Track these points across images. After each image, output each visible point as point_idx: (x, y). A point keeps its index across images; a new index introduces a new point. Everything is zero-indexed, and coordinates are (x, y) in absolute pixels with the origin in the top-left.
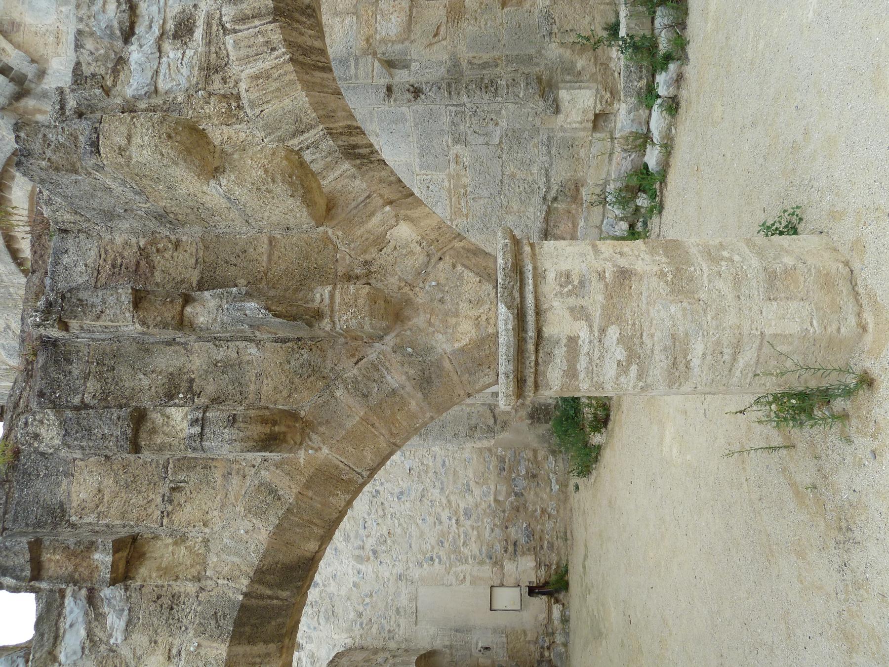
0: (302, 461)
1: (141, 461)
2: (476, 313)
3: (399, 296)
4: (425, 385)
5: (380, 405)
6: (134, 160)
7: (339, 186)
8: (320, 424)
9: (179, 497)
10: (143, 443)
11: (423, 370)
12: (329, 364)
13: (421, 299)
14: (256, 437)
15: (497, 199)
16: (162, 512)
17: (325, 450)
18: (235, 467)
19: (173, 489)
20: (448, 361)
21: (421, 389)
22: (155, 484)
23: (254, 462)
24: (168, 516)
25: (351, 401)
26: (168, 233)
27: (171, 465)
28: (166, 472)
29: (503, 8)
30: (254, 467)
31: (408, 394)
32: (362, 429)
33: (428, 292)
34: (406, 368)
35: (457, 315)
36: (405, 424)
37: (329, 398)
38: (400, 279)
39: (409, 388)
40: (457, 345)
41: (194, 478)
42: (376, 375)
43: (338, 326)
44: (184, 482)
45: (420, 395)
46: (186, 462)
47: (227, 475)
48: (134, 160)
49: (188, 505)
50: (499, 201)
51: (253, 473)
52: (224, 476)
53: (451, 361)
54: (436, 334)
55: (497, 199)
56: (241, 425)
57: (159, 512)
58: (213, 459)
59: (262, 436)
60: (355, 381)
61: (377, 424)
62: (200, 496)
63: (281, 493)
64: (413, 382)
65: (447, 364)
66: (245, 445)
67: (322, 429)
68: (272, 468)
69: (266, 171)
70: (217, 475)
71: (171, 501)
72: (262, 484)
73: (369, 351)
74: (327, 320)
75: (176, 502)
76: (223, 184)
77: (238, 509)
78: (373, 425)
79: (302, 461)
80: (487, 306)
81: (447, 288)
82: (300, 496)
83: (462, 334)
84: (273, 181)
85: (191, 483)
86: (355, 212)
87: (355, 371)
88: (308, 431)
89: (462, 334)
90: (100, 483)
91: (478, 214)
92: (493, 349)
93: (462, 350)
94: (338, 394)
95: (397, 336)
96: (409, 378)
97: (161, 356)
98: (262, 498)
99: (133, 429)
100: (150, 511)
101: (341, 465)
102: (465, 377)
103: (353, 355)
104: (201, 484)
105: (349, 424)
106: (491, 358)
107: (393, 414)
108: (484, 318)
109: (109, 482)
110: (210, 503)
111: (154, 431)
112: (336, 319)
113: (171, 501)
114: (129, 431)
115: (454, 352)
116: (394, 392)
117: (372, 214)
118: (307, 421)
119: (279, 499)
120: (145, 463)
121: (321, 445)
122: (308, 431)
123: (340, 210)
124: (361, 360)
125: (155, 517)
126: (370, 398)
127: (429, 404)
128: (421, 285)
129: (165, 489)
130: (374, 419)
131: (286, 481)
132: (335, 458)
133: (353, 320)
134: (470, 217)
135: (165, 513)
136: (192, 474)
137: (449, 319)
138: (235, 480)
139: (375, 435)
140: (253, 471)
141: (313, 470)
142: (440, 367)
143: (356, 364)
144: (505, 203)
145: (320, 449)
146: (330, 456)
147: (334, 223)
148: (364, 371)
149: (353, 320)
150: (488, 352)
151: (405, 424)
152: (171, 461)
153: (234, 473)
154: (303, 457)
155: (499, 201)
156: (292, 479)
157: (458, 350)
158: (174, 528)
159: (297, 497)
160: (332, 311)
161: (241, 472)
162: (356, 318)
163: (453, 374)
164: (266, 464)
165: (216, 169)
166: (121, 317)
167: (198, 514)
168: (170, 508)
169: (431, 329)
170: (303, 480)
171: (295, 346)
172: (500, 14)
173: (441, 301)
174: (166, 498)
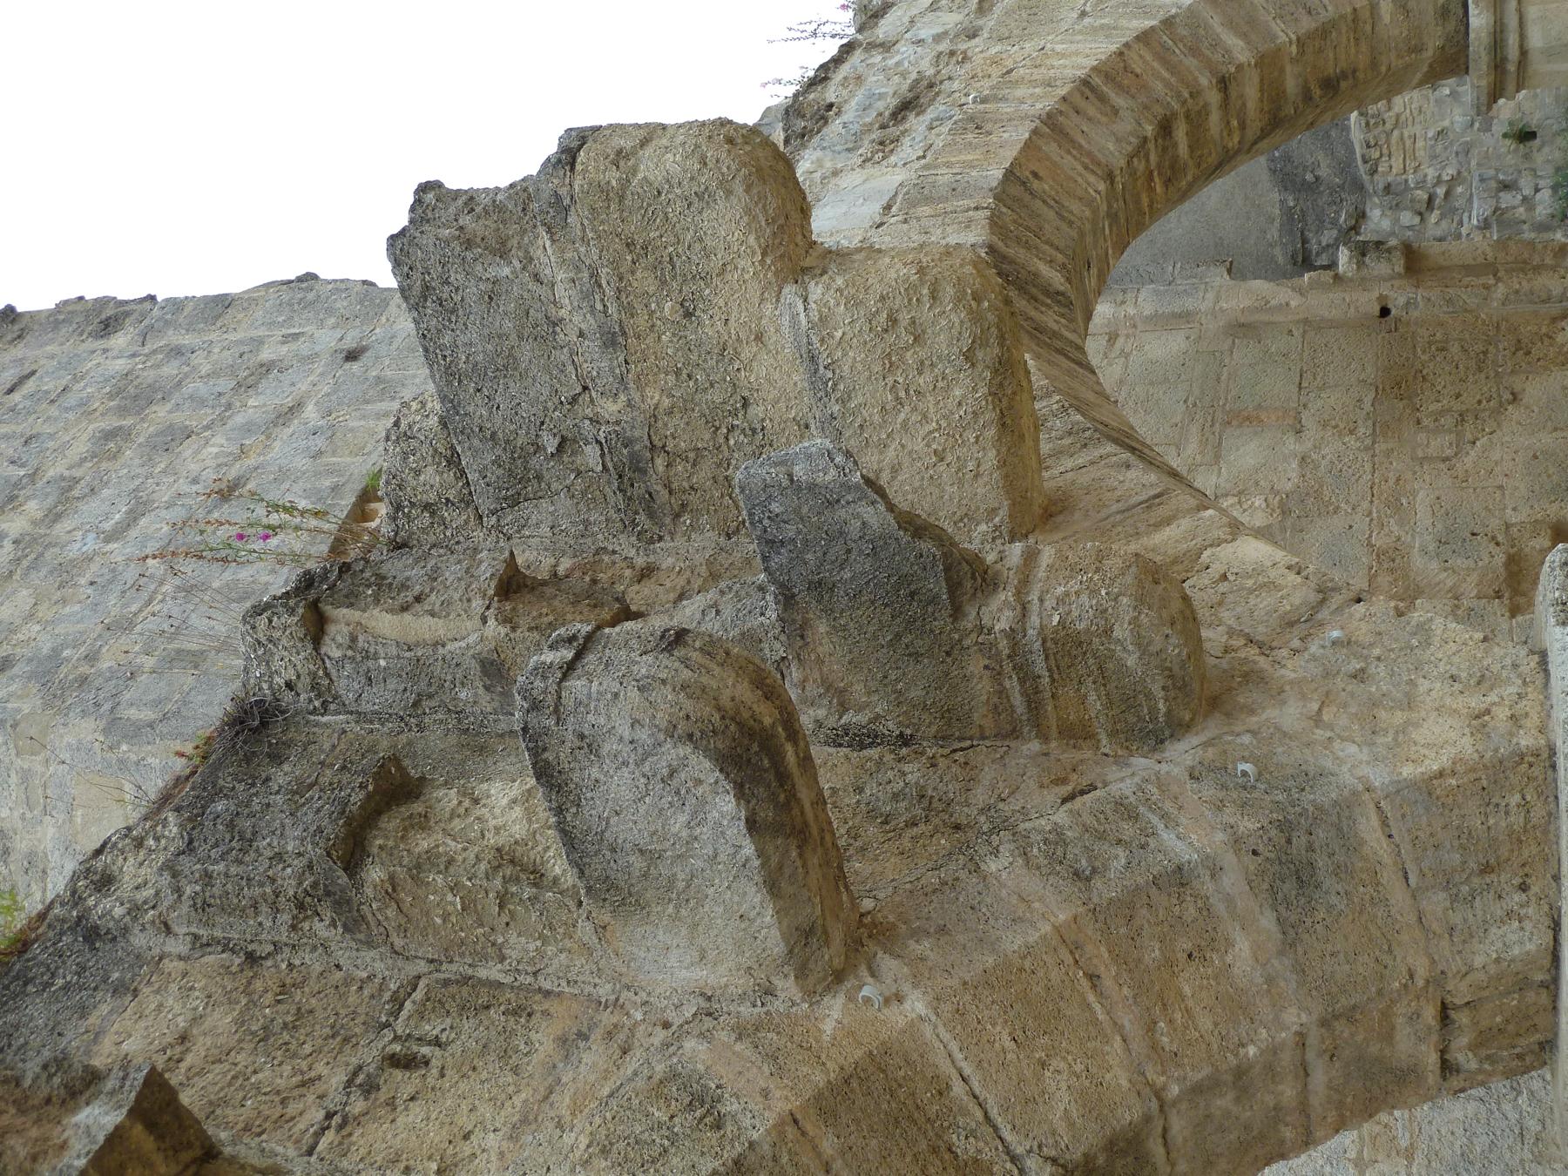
0: (828, 1027)
1: (339, 975)
2: (1476, 702)
3: (1224, 664)
4: (1289, 887)
5: (1126, 907)
6: (640, 176)
7: (1084, 478)
8: (917, 934)
9: (403, 1082)
10: (379, 842)
11: (1286, 827)
12: (980, 796)
13: (1292, 670)
14: (725, 700)
15: (1507, 1107)
16: (329, 1116)
17: (917, 1004)
18: (607, 1018)
19: (395, 1061)
20: (1375, 821)
21: (1275, 899)
22: (346, 1040)
23: (671, 1015)
24: (341, 1127)
25: (1032, 884)
26: (633, 553)
27: (418, 995)
28: (396, 1014)
29: (1513, 616)
30: (666, 1025)
31: (1229, 900)
32: (1055, 975)
33: (1314, 658)
34: (1230, 815)
35: (1410, 703)
36: (1205, 1023)
37: (962, 874)
38: (1231, 633)
39: (1233, 881)
40: (1407, 771)
41: (468, 1034)
42: (1128, 830)
43: (1034, 620)
44: (437, 1042)
45: (1268, 921)
46: (465, 990)
47: (570, 1043)
48: (640, 176)
49: (417, 1111)
50: (1513, 1116)
51: (657, 1041)
52: (563, 1041)
53: (1384, 823)
54: (1337, 745)
55: (1507, 1107)
56: (695, 655)
57: (321, 1114)
58: (547, 994)
59: (746, 715)
60: (1056, 838)
61: (1108, 982)
62: (463, 1086)
63: (730, 1106)
64: (1252, 863)
65: (1368, 826)
66: (688, 705)
67: (924, 947)
68: (723, 1036)
69: (921, 271)
70: (543, 1039)
71: (369, 1088)
72: (676, 1075)
73: (1113, 773)
74: (1005, 595)
75: (383, 1096)
76: (812, 298)
77: (569, 1139)
78: (1093, 978)
79: (828, 1027)
80: (1513, 690)
81: (1377, 652)
82: (791, 1132)
83: (1428, 746)
84: (934, 297)
85: (456, 1048)
86: (1118, 517)
87: (1062, 817)
88: (871, 947)
89: (1428, 746)
90: (196, 1020)
91: (1446, 1153)
92: (1538, 813)
93: (1427, 787)
94: (992, 866)
95: (1206, 745)
96: (1237, 841)
97: (513, 759)
98: (660, 1115)
99: (369, 796)
100: (292, 1109)
101: (958, 1088)
102: (1436, 902)
103: (1063, 781)
104: (482, 1055)
105: (1013, 942)
106: (1529, 850)
107: (1169, 963)
108: (1502, 713)
109: (222, 1020)
110: (486, 1110)
111: (423, 823)
112: (1034, 597)
113: (369, 1088)
114: (357, 797)
115: (1400, 789)
116: (1179, 878)
117: (1167, 521)
118: (874, 924)
119: (718, 1125)
120: (348, 981)
121: (906, 988)
122: (871, 947)
123: (1077, 515)
124: (1083, 793)
125: (302, 1126)
126: (1097, 882)
127: (1300, 970)
128: (1296, 643)
129: (368, 1054)
130: (1099, 955)
131: (760, 1075)
132: (946, 1051)
133: (1084, 598)
134: (1419, 1158)
135: (337, 1119)
136: (467, 1025)
137: (1382, 714)
138: (593, 1056)
139: (1095, 1022)
140: (660, 1035)
141: (859, 1053)
142: (1347, 839)
143: (1064, 801)
144: (1533, 1125)
145: (900, 999)
146: (928, 1031)
147: (1057, 536)
148: (1089, 820)
149: (1084, 598)
150: (1517, 820)
151: (1205, 1023)
152: (421, 984)
153: (597, 1035)
154: (836, 1014)
155: (1513, 1116)
156: (779, 1072)
157: (1412, 784)
158: (345, 1164)
159: (779, 1127)
160: (1025, 582)
161: (622, 1037)
162: (1094, 593)
163: (1389, 877)
164: (708, 1023)
165: (804, 270)
166: (458, 607)
167: (436, 1136)
168: (358, 1105)
169: (1320, 734)
170: (819, 1079)
171: (889, 757)
172: (1505, 626)
173: (1359, 676)
174: (360, 1079)
